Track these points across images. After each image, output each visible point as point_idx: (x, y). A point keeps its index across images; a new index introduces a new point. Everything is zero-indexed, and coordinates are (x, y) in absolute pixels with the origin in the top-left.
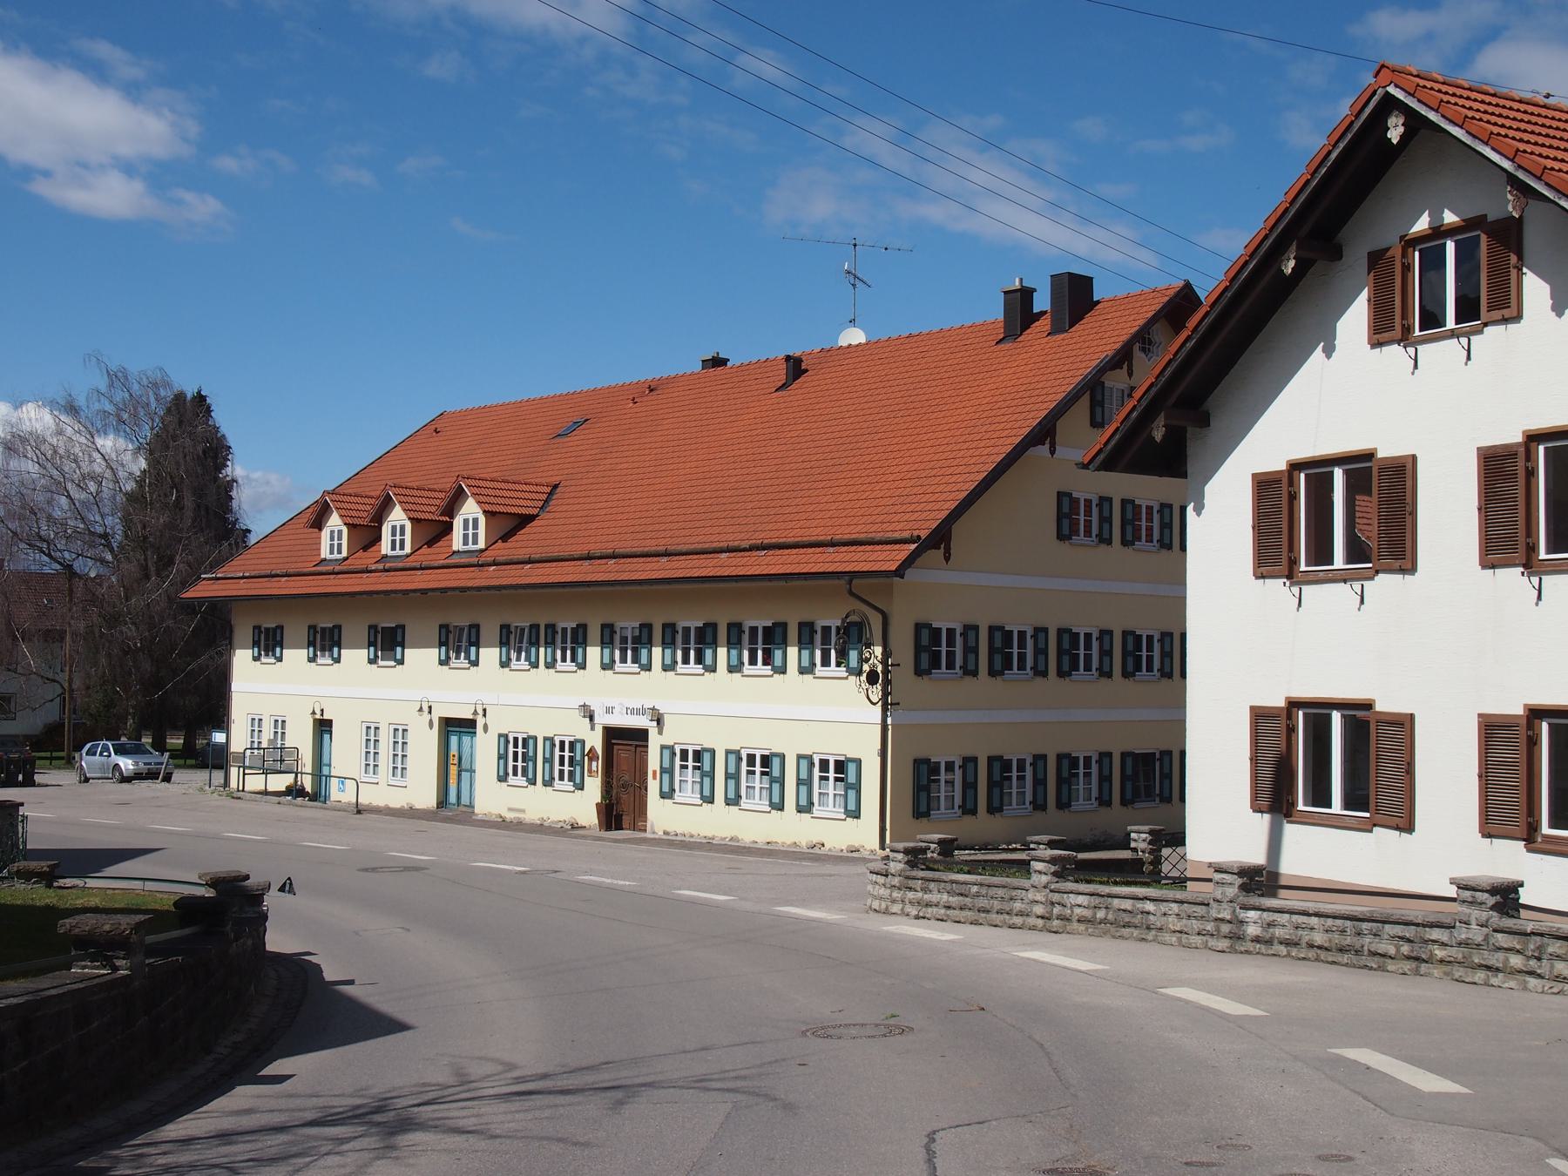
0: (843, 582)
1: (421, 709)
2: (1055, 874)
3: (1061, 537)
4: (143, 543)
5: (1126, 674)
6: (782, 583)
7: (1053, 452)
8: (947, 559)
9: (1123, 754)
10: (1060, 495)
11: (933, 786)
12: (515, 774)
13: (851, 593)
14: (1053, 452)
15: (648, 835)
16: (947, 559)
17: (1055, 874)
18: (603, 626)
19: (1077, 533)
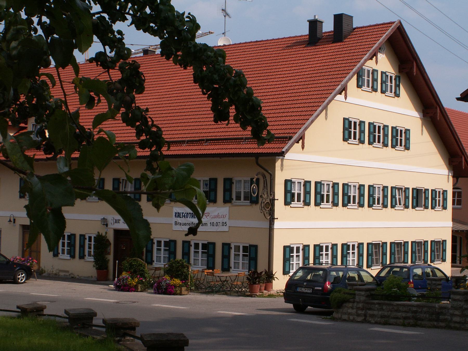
0: (254, 158)
1: (10, 221)
2: (367, 296)
3: (345, 140)
4: (181, 31)
5: (370, 206)
6: (218, 159)
7: (346, 98)
8: (303, 148)
9: (412, 242)
10: (344, 119)
11: (321, 257)
12: (63, 253)
13: (258, 164)
14: (346, 98)
15: (272, 292)
16: (303, 148)
17: (367, 296)
18: (114, 180)
19: (350, 138)
